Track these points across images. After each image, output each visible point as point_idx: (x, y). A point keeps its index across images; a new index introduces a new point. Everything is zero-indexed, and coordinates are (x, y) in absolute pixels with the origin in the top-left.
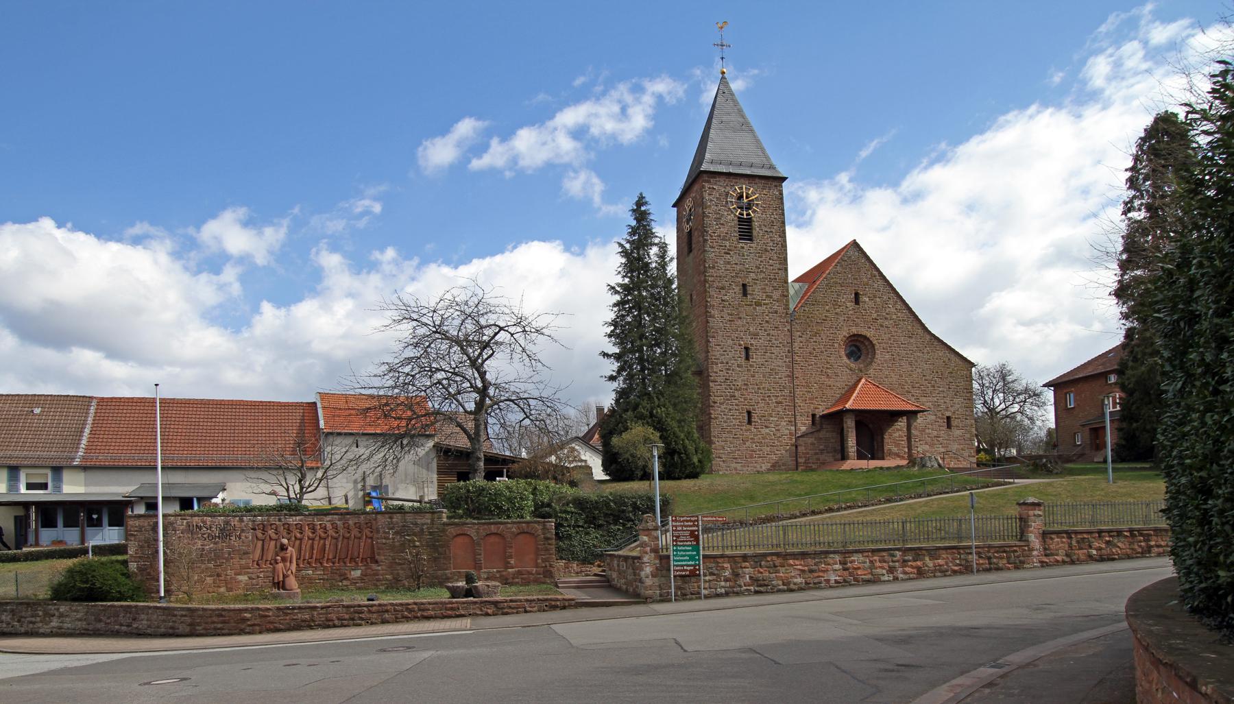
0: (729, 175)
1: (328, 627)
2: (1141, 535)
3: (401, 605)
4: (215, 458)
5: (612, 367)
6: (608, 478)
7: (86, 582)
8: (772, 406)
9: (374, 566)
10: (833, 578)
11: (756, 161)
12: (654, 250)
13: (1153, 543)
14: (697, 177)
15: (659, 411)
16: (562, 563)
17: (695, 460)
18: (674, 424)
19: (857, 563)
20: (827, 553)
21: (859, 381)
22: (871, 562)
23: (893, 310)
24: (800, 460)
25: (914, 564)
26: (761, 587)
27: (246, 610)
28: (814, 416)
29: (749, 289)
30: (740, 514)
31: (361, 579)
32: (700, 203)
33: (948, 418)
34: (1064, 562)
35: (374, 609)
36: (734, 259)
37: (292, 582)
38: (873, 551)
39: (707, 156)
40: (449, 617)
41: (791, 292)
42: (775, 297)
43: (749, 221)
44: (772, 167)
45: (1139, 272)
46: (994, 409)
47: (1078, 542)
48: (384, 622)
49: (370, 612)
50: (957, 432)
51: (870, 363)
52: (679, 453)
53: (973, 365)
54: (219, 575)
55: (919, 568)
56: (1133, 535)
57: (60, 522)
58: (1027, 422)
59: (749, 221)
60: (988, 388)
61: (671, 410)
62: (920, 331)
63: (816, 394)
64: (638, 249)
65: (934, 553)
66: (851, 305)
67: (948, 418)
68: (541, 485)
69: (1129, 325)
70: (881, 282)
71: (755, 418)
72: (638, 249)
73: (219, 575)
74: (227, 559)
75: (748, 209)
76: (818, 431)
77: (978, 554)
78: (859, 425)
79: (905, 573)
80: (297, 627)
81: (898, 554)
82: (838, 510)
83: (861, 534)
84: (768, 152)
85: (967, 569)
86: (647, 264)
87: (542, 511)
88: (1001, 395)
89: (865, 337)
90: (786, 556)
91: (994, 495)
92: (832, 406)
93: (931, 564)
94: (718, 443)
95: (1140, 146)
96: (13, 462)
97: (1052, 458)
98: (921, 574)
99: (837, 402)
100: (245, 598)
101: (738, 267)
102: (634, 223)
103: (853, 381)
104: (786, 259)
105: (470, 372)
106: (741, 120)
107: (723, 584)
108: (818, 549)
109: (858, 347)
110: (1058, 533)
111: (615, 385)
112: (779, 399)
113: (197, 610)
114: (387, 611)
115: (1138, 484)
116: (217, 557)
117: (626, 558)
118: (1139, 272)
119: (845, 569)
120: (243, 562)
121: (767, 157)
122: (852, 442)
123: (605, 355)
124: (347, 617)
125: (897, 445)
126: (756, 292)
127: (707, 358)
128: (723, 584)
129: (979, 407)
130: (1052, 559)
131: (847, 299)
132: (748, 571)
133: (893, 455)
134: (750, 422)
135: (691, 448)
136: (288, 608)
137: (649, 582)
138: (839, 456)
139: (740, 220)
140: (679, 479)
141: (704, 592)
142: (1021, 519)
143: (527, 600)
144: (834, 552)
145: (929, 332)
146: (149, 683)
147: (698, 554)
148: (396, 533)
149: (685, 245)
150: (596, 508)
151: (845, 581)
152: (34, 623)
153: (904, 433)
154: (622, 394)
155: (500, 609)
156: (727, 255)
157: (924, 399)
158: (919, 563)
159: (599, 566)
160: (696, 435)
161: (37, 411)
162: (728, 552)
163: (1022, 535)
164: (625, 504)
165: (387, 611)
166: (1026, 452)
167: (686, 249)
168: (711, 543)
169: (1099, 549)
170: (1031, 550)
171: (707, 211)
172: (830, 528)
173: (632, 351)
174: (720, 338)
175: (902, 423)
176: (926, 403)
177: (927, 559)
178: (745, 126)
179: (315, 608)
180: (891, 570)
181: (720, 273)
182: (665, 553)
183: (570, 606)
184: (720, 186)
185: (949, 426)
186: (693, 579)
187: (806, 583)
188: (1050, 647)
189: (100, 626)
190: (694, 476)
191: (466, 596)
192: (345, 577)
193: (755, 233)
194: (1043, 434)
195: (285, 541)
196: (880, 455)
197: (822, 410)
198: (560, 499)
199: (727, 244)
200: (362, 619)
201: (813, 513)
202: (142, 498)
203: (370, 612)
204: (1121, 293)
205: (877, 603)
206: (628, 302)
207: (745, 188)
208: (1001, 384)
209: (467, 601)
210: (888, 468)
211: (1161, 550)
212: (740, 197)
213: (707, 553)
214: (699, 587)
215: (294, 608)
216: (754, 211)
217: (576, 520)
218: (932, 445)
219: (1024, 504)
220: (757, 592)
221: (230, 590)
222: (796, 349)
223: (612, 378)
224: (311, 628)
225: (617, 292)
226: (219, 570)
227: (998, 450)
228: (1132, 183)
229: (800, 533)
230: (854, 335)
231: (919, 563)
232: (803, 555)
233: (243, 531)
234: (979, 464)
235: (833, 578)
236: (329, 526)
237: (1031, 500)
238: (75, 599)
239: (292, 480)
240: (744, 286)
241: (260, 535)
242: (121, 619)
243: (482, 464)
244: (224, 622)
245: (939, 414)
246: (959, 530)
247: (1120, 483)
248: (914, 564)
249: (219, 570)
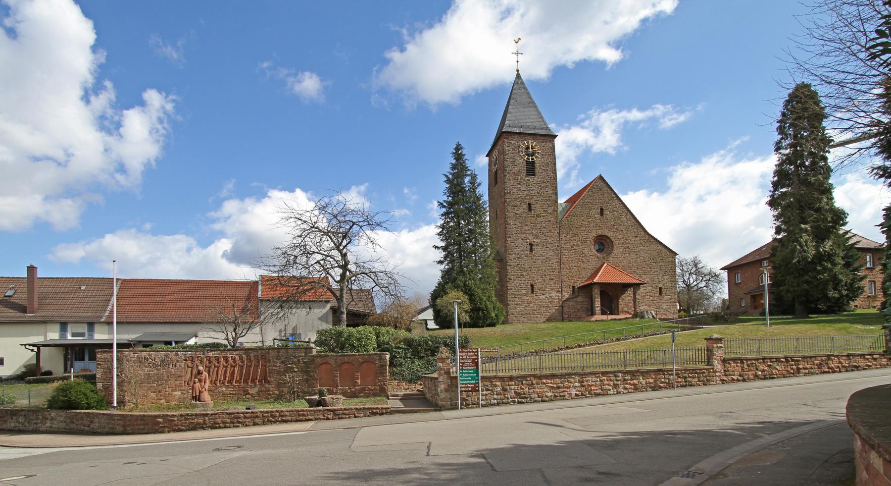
0: (520, 134)
1: (216, 428)
2: (792, 360)
3: (267, 412)
4: (191, 317)
5: (440, 255)
7: (65, 397)
9: (267, 385)
10: (574, 392)
11: (538, 125)
12: (467, 179)
13: (801, 366)
14: (501, 135)
16: (396, 382)
17: (493, 315)
18: (480, 291)
19: (590, 383)
20: (570, 375)
22: (601, 381)
25: (632, 382)
26: (522, 399)
27: (159, 416)
28: (574, 287)
30: (517, 349)
31: (258, 393)
32: (503, 153)
33: (660, 288)
34: (738, 380)
35: (248, 415)
36: (524, 187)
37: (206, 396)
38: (603, 374)
39: (507, 122)
40: (301, 421)
41: (560, 209)
44: (548, 129)
45: (784, 190)
47: (748, 366)
48: (255, 424)
49: (245, 417)
52: (483, 310)
53: (676, 254)
54: (160, 392)
55: (634, 385)
56: (787, 361)
57: (87, 357)
58: (710, 293)
59: (533, 163)
62: (642, 233)
64: (457, 178)
65: (646, 374)
66: (598, 216)
67: (660, 288)
68: (383, 330)
69: (778, 224)
70: (617, 201)
71: (536, 289)
72: (457, 178)
73: (160, 392)
74: (166, 381)
75: (532, 155)
77: (677, 374)
78: (603, 294)
79: (625, 388)
80: (194, 428)
81: (620, 374)
82: (584, 346)
84: (546, 120)
85: (670, 386)
86: (463, 188)
87: (382, 347)
89: (607, 237)
90: (540, 377)
91: (688, 335)
94: (512, 305)
95: (786, 106)
96: (63, 320)
97: (727, 315)
98: (636, 389)
99: (589, 279)
100: (179, 407)
102: (454, 162)
104: (556, 187)
105: (335, 253)
108: (564, 371)
109: (603, 244)
110: (734, 360)
111: (442, 267)
113: (127, 416)
114: (257, 417)
115: (787, 327)
116: (159, 379)
117: (432, 378)
118: (784, 190)
119: (583, 386)
120: (178, 382)
121: (545, 123)
122: (598, 303)
123: (436, 247)
124: (229, 421)
125: (627, 306)
126: (537, 208)
129: (681, 284)
130: (730, 378)
131: (595, 212)
132: (513, 387)
133: (623, 312)
134: (532, 292)
135: (490, 306)
136: (188, 415)
137: (442, 395)
139: (528, 163)
140: (483, 327)
142: (708, 350)
143: (356, 409)
144: (575, 374)
145: (648, 234)
146: (28, 477)
147: (478, 376)
148: (282, 362)
149: (493, 180)
150: (419, 345)
151: (582, 394)
152: (36, 424)
154: (446, 274)
155: (337, 415)
156: (518, 186)
160: (494, 299)
161: (83, 288)
162: (500, 374)
163: (709, 362)
164: (439, 342)
165: (257, 417)
166: (709, 311)
168: (485, 370)
169: (763, 371)
171: (506, 157)
172: (572, 360)
175: (630, 292)
177: (641, 378)
178: (532, 104)
179: (206, 415)
180: (615, 386)
182: (455, 375)
183: (386, 413)
184: (514, 142)
185: (661, 294)
186: (474, 393)
187: (555, 396)
188: (737, 452)
189: (73, 426)
190: (492, 325)
191: (318, 406)
192: (246, 392)
193: (536, 171)
194: (720, 303)
195: (201, 368)
197: (579, 284)
198: (395, 339)
200: (239, 422)
201: (567, 348)
202: (140, 342)
203: (245, 417)
204: (773, 203)
205: (600, 411)
206: (451, 213)
207: (530, 142)
209: (320, 408)
210: (620, 319)
211: (807, 371)
214: (478, 399)
215: (192, 415)
219: (711, 339)
220: (519, 403)
221: (168, 401)
222: (563, 245)
223: (441, 262)
224: (204, 428)
226: (160, 388)
227: (691, 312)
228: (781, 130)
229: (550, 363)
232: (553, 376)
233: (177, 361)
234: (680, 317)
235: (574, 392)
236: (237, 357)
237: (715, 336)
238: (61, 408)
239: (231, 328)
240: (530, 204)
241: (190, 364)
242: (85, 422)
243: (345, 316)
244: (144, 425)
246: (664, 359)
247: (774, 327)
248: (632, 382)
249: (160, 388)
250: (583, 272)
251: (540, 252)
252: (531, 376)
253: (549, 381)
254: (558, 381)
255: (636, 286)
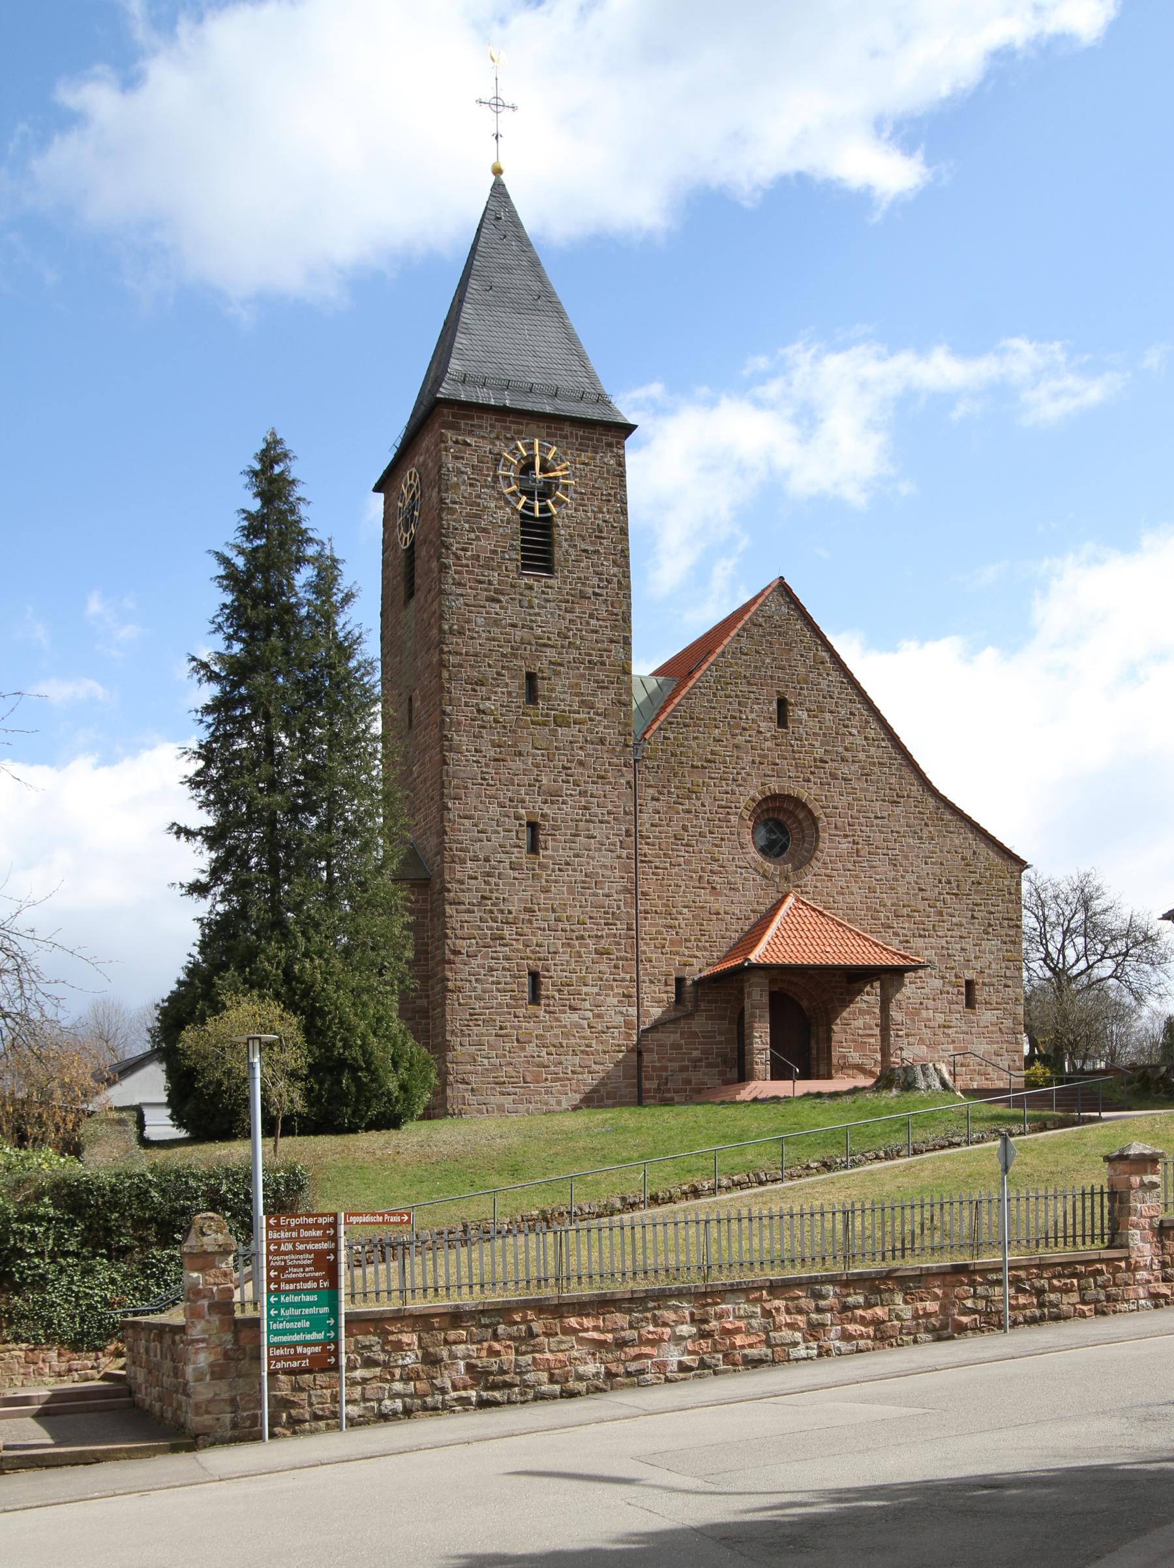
5: (197, 860)
6: (182, 1134)
8: (587, 959)
11: (564, 382)
12: (305, 575)
14: (434, 414)
15: (310, 969)
17: (392, 1085)
18: (344, 999)
21: (781, 902)
22: (767, 1314)
23: (859, 740)
24: (647, 1085)
25: (868, 1314)
26: (492, 1390)
28: (680, 981)
29: (542, 686)
30: (477, 1209)
32: (436, 480)
33: (970, 984)
36: (511, 613)
39: (455, 365)
42: (601, 707)
43: (547, 524)
44: (602, 400)
46: (1064, 971)
50: (987, 1016)
51: (806, 861)
52: (354, 1069)
55: (877, 1323)
58: (1129, 1000)
60: (1054, 926)
61: (337, 963)
62: (916, 789)
63: (685, 932)
64: (265, 569)
67: (970, 984)
70: (835, 676)
71: (547, 988)
72: (265, 569)
75: (544, 495)
76: (689, 1016)
77: (1016, 1282)
79: (846, 1337)
81: (829, 1289)
83: (756, 1243)
85: (992, 1321)
86: (289, 609)
88: (1080, 941)
90: (559, 1309)
92: (722, 960)
93: (907, 1312)
94: (461, 1049)
98: (883, 1337)
101: (519, 634)
102: (255, 505)
103: (769, 903)
104: (627, 619)
106: (536, 286)
107: (398, 1386)
109: (784, 828)
112: (604, 944)
117: (162, 1329)
119: (704, 1335)
122: (761, 1037)
125: (861, 1046)
126: (559, 691)
127: (441, 848)
128: (398, 1386)
132: (464, 1350)
134: (535, 999)
135: (381, 1052)
137: (203, 1391)
138: (734, 1074)
140: (353, 1130)
141: (348, 1410)
142: (1113, 1195)
144: (680, 1294)
147: (334, 1312)
150: (114, 1205)
151: (703, 1365)
153: (873, 1020)
156: (492, 611)
157: (919, 943)
158: (880, 1312)
159: (118, 1354)
162: (417, 1304)
163: (1116, 1236)
166: (1125, 1061)
167: (401, 591)
168: (365, 1288)
170: (1132, 1268)
171: (449, 497)
172: (668, 1242)
173: (247, 823)
174: (472, 801)
175: (870, 998)
176: (923, 950)
177: (899, 1298)
180: (814, 1330)
181: (475, 646)
182: (250, 1313)
184: (481, 441)
185: (970, 1003)
186: (322, 1379)
187: (610, 1375)
190: (389, 1122)
193: (558, 554)
196: (823, 1070)
197: (698, 969)
199: (495, 577)
208: (1080, 916)
212: (527, 467)
213: (361, 1308)
214: (335, 1399)
216: (559, 503)
217: (59, 1237)
218: (932, 1046)
219: (1122, 1158)
220: (483, 1404)
222: (645, 828)
225: (213, 677)
230: (774, 797)
231: (880, 1312)
232: (603, 1304)
234: (1030, 1084)
235: (673, 1356)
240: (531, 678)
245: (950, 976)
246: (975, 1231)
248: (868, 1314)
250: (714, 928)
251: (564, 854)
252: (525, 1305)
253: (588, 1322)
254: (621, 1319)
255: (890, 977)
